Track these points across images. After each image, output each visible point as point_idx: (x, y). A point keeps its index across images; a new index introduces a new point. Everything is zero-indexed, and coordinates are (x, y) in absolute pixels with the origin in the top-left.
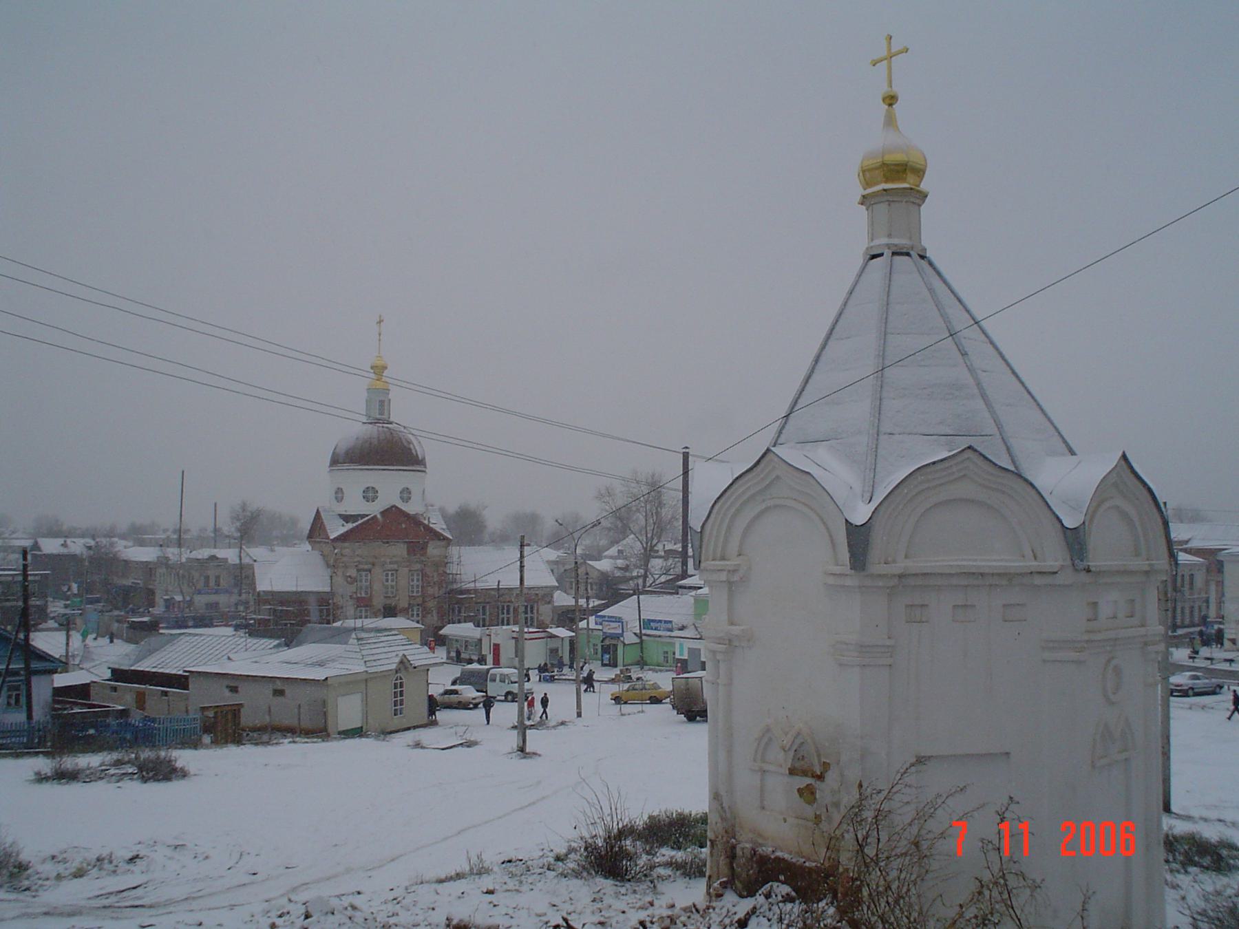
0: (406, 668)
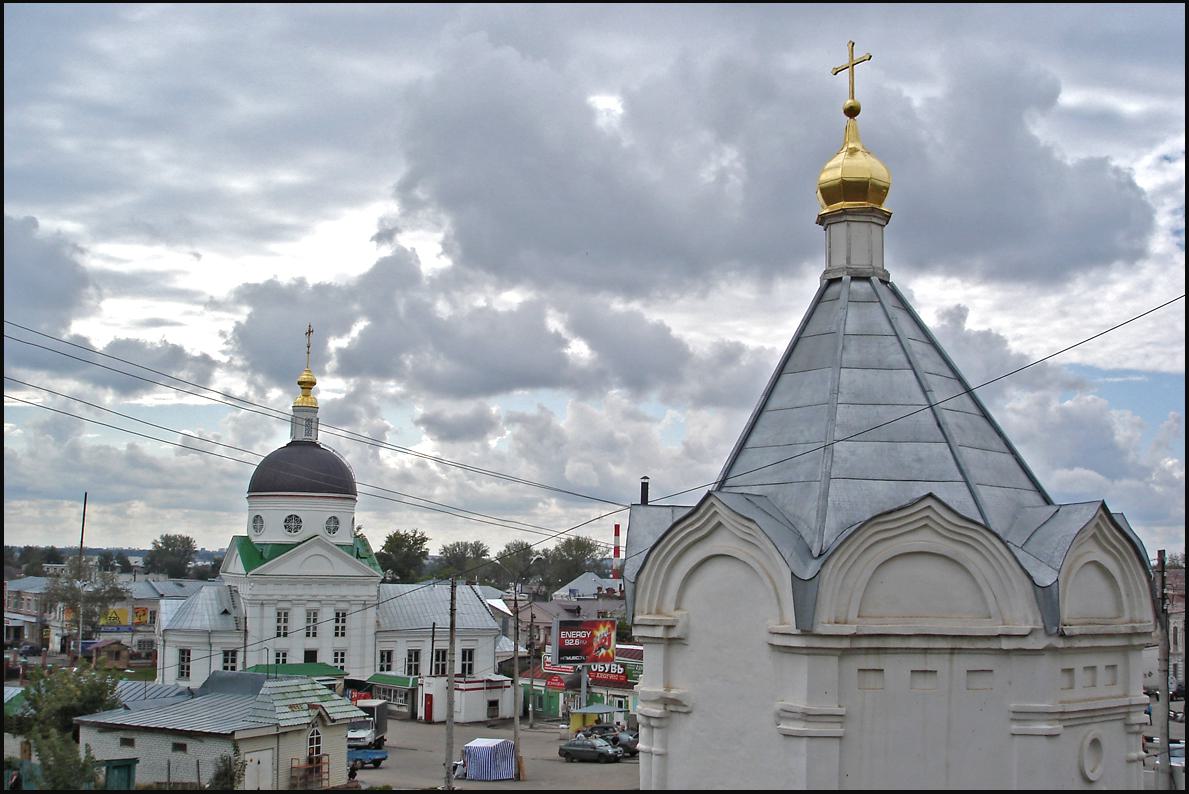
0: (323, 720)
